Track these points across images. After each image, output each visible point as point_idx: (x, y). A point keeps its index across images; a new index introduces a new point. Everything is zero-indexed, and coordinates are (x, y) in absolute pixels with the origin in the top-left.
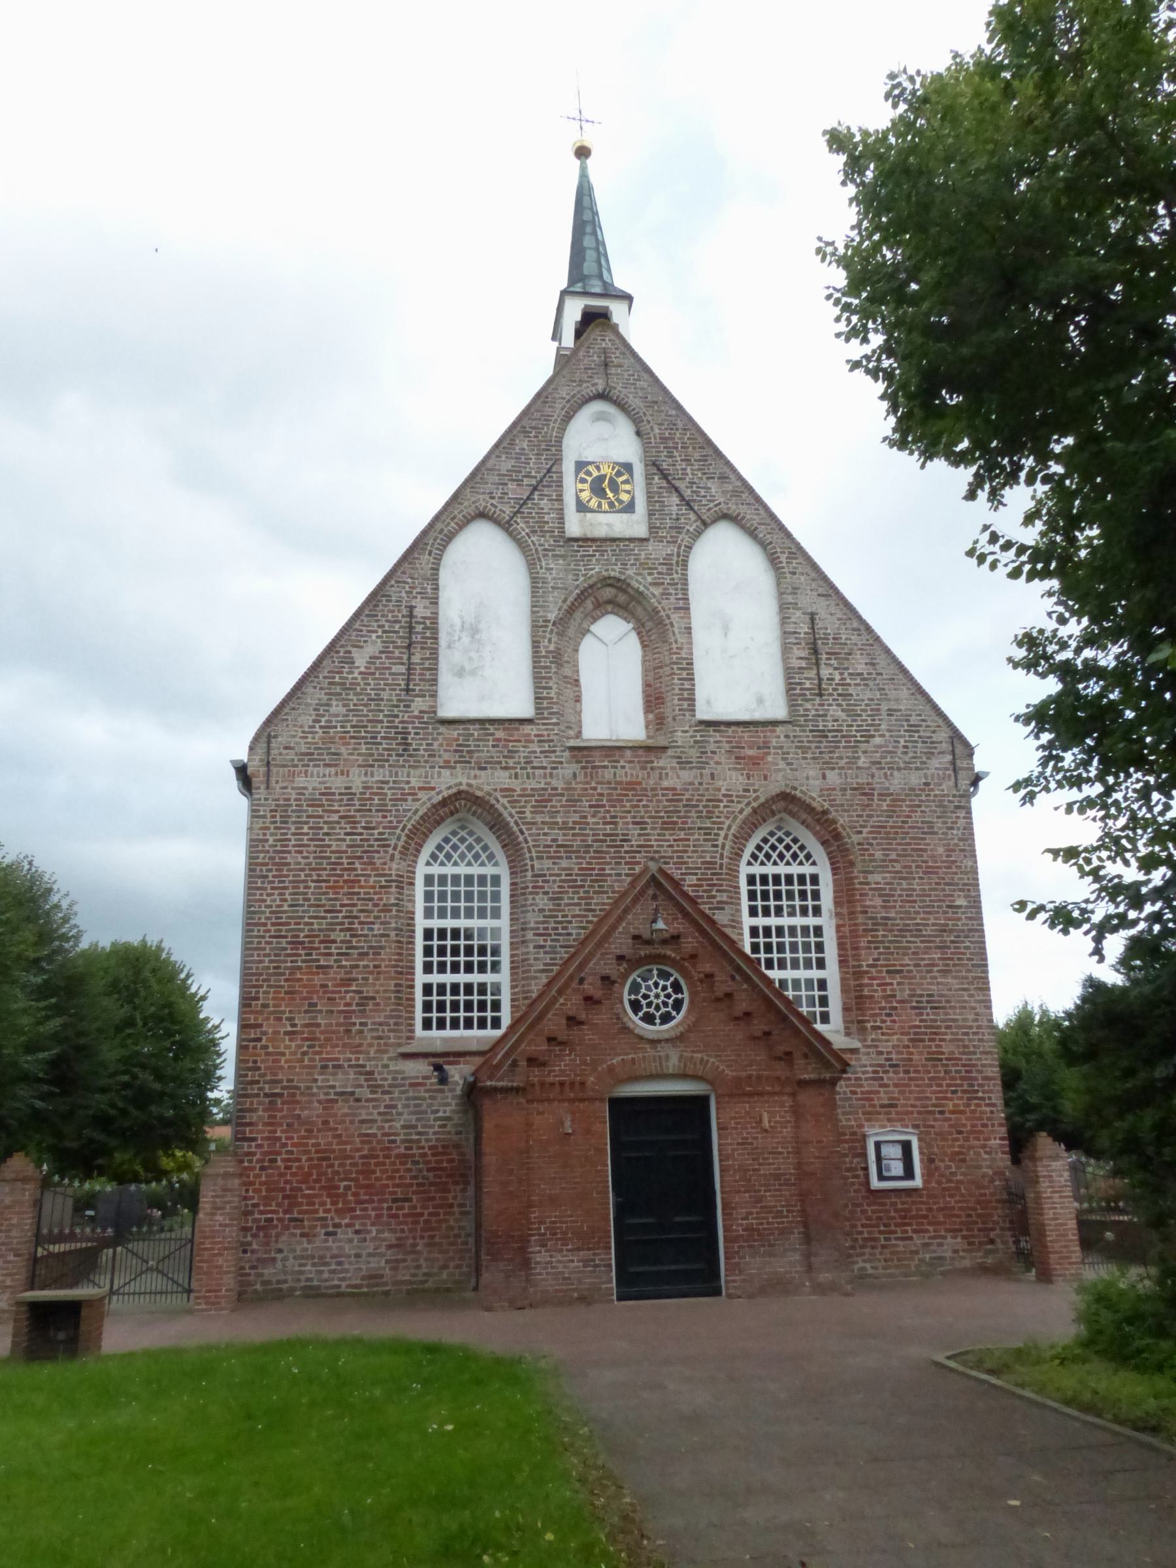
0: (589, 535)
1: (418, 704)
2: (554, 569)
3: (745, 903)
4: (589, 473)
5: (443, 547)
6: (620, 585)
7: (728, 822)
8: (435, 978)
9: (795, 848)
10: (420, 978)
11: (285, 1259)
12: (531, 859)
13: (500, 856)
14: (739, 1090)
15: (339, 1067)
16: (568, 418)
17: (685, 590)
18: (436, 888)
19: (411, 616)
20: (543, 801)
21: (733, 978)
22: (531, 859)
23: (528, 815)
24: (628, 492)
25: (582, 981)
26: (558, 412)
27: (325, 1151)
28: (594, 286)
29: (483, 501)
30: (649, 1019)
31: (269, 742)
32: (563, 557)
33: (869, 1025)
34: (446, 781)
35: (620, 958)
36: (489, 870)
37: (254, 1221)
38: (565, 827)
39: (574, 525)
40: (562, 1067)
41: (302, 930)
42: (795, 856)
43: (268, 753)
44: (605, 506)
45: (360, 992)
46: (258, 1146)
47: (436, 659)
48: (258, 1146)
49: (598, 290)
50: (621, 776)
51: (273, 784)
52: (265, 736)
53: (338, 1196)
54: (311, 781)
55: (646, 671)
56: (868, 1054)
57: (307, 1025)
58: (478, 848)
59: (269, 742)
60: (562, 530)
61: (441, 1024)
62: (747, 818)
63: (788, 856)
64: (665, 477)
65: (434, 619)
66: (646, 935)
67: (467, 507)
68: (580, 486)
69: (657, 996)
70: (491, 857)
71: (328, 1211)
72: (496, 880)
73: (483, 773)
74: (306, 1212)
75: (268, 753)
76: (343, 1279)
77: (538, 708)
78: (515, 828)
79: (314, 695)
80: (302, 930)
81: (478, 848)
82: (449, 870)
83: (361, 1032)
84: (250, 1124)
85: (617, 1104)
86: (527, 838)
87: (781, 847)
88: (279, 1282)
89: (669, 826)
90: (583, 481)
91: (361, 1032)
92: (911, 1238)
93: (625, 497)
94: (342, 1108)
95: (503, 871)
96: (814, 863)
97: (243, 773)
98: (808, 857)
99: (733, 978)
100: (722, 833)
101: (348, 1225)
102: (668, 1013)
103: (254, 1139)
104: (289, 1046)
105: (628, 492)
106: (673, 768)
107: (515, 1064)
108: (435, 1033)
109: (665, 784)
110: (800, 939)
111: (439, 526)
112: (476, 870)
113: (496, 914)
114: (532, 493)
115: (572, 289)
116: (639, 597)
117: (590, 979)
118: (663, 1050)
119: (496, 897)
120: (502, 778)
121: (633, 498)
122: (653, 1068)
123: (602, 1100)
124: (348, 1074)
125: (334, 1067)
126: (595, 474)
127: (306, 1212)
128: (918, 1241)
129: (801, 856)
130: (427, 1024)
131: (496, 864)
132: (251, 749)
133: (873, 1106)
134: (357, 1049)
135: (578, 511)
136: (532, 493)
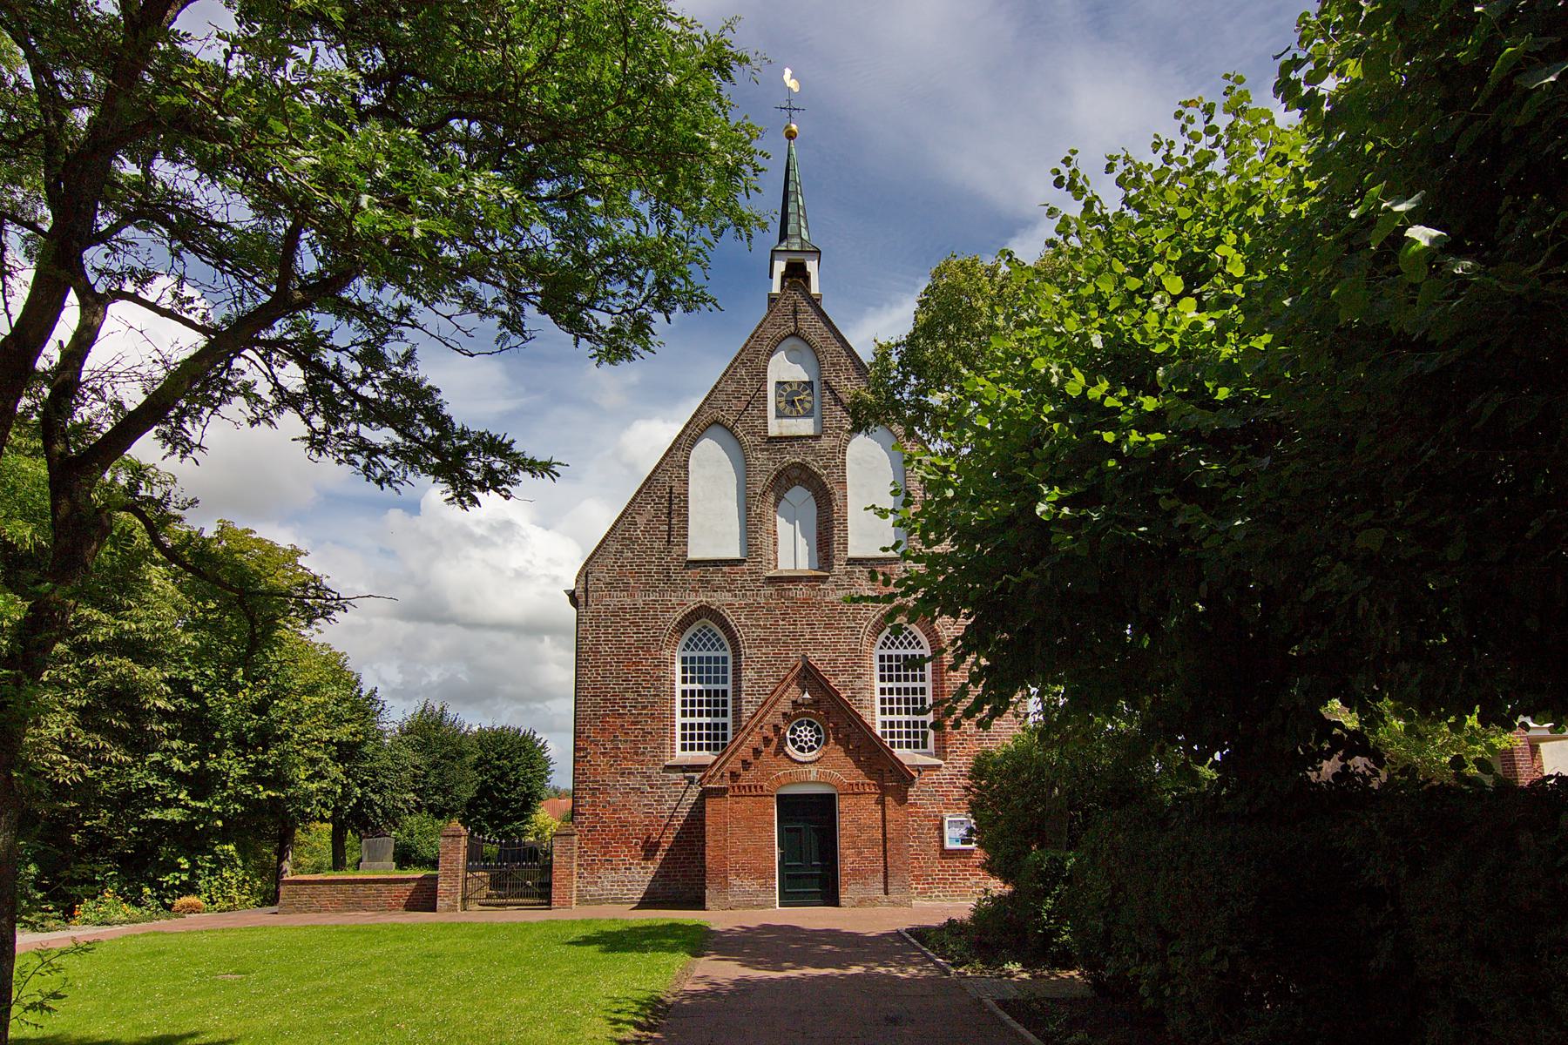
0: (784, 435)
1: (676, 551)
2: (760, 458)
3: (877, 673)
4: (785, 390)
5: (692, 446)
6: (803, 467)
7: (866, 623)
8: (688, 720)
9: (910, 638)
10: (679, 720)
11: (603, 882)
12: (744, 648)
13: (729, 649)
14: (854, 792)
15: (633, 773)
16: (771, 353)
17: (844, 470)
18: (689, 698)
19: (671, 492)
20: (752, 609)
21: (850, 725)
22: (744, 648)
23: (743, 620)
24: (809, 402)
25: (762, 727)
26: (764, 350)
27: (624, 822)
28: (794, 244)
29: (718, 414)
30: (801, 749)
31: (586, 577)
32: (767, 450)
33: (948, 750)
34: (693, 601)
35: (784, 714)
36: (721, 654)
37: (585, 860)
38: (765, 627)
39: (775, 427)
40: (747, 778)
41: (609, 692)
42: (910, 643)
43: (587, 583)
44: (794, 414)
45: (643, 729)
46: (586, 818)
47: (687, 521)
48: (586, 818)
49: (796, 248)
50: (800, 595)
51: (590, 602)
52: (585, 573)
53: (631, 847)
54: (616, 599)
55: (819, 525)
56: (947, 768)
57: (613, 749)
58: (714, 640)
59: (586, 577)
60: (766, 431)
61: (692, 748)
62: (878, 620)
63: (906, 643)
64: (832, 391)
65: (686, 495)
66: (800, 701)
67: (705, 419)
68: (779, 399)
69: (806, 736)
70: (722, 645)
71: (626, 856)
72: (725, 660)
73: (715, 594)
74: (613, 856)
75: (587, 583)
76: (635, 894)
77: (749, 554)
78: (735, 629)
79: (614, 546)
80: (609, 692)
81: (714, 640)
82: (697, 654)
83: (644, 753)
84: (582, 806)
85: (781, 798)
86: (741, 634)
87: (705, 640)
88: (599, 895)
89: (828, 626)
90: (781, 395)
91: (644, 753)
92: (968, 879)
93: (807, 406)
94: (633, 797)
95: (729, 654)
96: (922, 648)
97: (573, 597)
98: (918, 643)
99: (850, 725)
100: (862, 630)
101: (637, 864)
102: (804, 748)
103: (585, 814)
104: (602, 761)
105: (809, 402)
106: (832, 590)
107: (722, 776)
108: (688, 753)
109: (827, 599)
110: (911, 696)
111: (689, 431)
112: (712, 654)
113: (725, 681)
114: (747, 406)
115: (779, 248)
116: (814, 476)
117: (766, 727)
118: (807, 768)
119: (725, 670)
120: (727, 597)
121: (813, 406)
122: (803, 777)
123: (772, 796)
124: (295, 811)
125: (629, 773)
126: (789, 390)
127: (613, 856)
128: (973, 880)
129: (914, 643)
130: (684, 748)
131: (725, 650)
132: (577, 581)
133: (949, 800)
134: (641, 763)
135: (777, 417)
136: (747, 406)
